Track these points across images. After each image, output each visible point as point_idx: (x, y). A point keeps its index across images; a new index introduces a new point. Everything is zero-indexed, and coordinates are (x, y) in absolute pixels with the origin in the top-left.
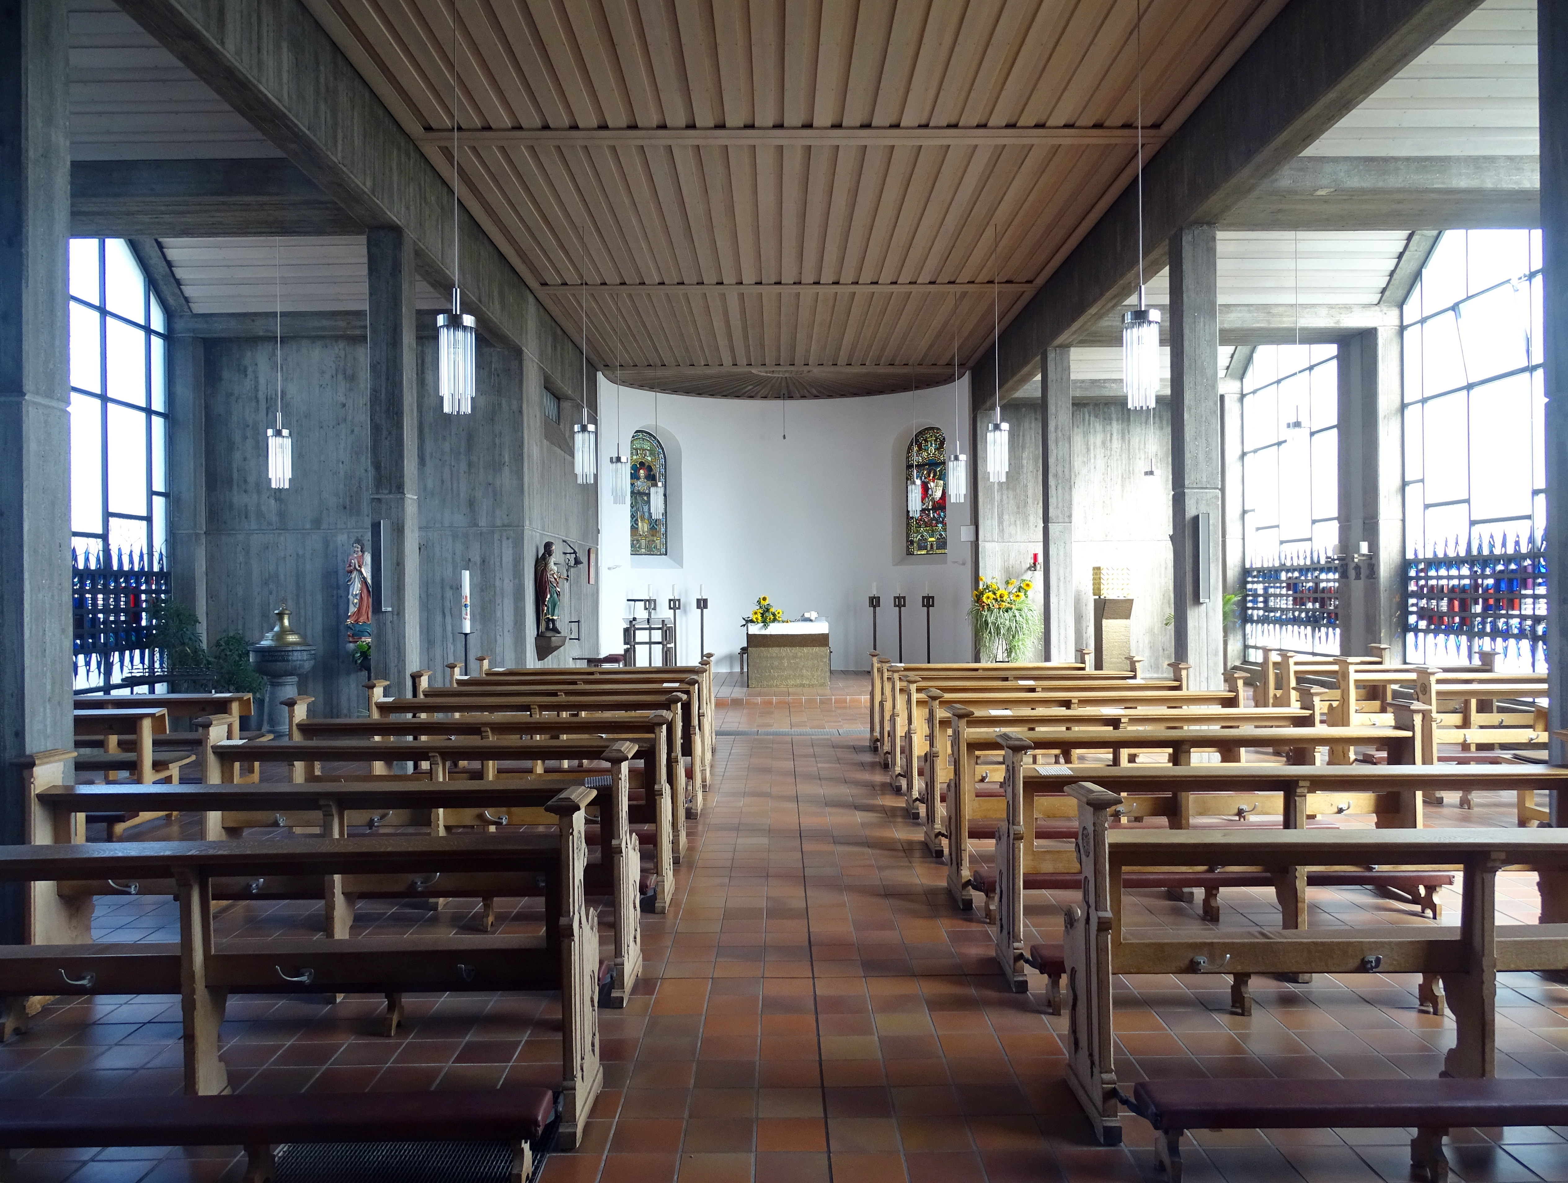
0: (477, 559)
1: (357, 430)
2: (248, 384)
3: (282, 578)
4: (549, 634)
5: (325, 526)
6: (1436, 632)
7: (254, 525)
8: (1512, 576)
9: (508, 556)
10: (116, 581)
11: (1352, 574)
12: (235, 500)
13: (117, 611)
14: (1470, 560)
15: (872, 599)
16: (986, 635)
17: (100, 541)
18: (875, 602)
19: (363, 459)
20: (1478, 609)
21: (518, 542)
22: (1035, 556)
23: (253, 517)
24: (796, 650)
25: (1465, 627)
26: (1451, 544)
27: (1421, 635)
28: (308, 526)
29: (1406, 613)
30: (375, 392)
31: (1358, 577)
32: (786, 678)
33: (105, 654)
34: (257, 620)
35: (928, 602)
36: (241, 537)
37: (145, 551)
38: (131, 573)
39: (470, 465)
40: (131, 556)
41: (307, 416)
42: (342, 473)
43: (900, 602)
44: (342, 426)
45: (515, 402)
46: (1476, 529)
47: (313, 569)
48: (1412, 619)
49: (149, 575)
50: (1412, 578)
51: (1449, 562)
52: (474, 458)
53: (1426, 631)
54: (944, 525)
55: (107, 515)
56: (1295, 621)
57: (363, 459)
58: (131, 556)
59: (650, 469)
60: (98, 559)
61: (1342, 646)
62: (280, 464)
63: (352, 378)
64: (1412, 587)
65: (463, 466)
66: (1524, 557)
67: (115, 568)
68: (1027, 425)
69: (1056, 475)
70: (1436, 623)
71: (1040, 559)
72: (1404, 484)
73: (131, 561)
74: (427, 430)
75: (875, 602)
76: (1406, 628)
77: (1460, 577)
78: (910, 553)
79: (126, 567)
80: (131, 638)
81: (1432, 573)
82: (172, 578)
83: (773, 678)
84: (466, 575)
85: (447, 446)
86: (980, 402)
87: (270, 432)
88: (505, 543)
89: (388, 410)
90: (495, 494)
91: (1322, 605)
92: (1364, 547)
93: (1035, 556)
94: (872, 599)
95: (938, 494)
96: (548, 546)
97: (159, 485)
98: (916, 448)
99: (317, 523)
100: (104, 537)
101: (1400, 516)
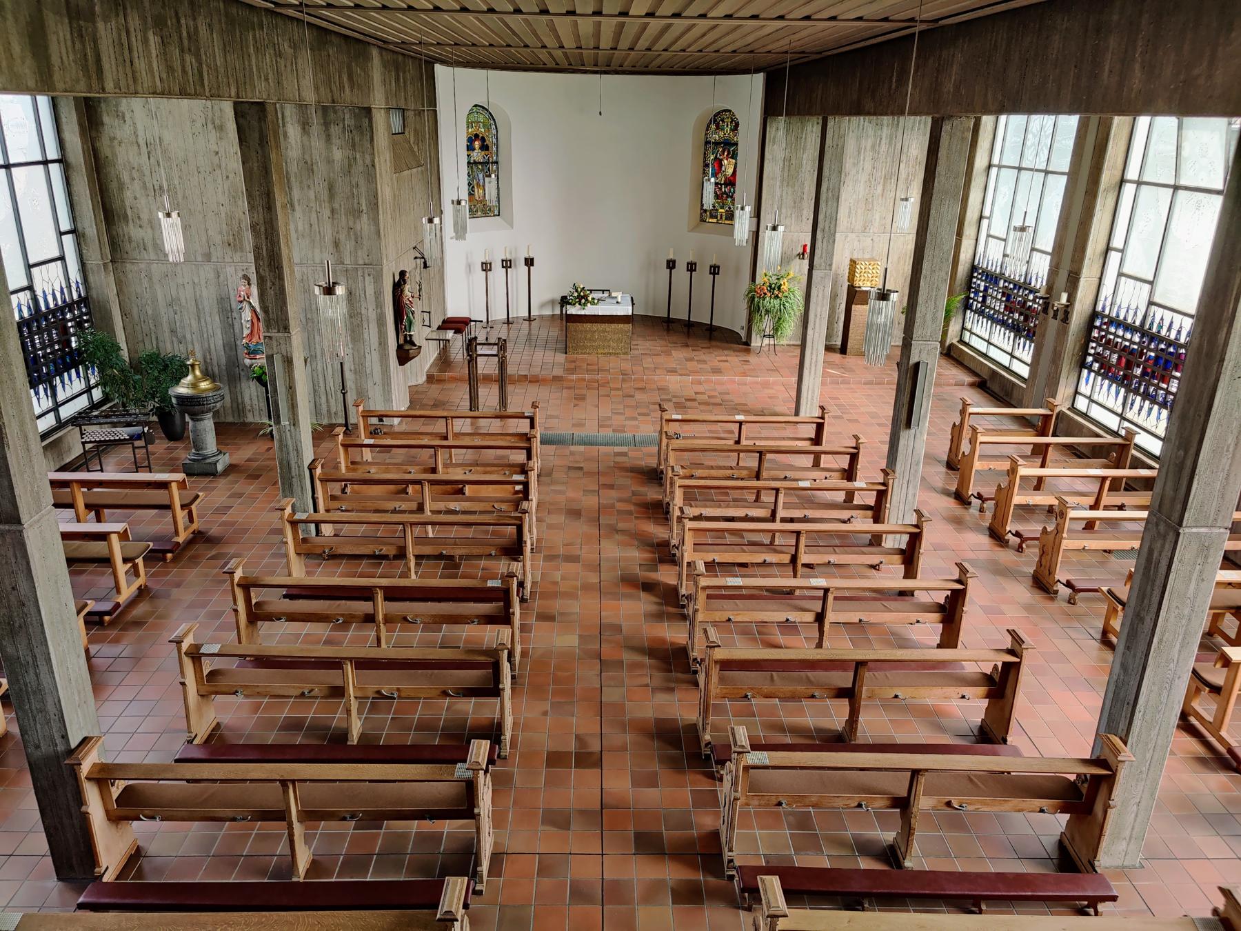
3: (183, 301)
4: (407, 347)
5: (214, 259)
6: (1105, 377)
7: (153, 256)
8: (1169, 357)
9: (370, 290)
10: (46, 319)
11: (1051, 313)
12: (133, 234)
14: (1142, 330)
15: (668, 262)
16: (757, 316)
17: (28, 292)
18: (671, 264)
19: (240, 203)
20: (1138, 371)
21: (378, 279)
22: (805, 246)
23: (150, 249)
24: (604, 326)
25: (1124, 381)
26: (1131, 313)
27: (1093, 374)
28: (200, 259)
29: (1086, 354)
30: (257, 249)
31: (1055, 317)
34: (167, 334)
35: (715, 270)
36: (143, 266)
39: (333, 211)
40: (54, 294)
41: (186, 161)
42: (223, 215)
43: (691, 267)
44: (218, 172)
45: (367, 157)
46: (1154, 308)
47: (209, 296)
48: (1090, 359)
49: (70, 306)
51: (1128, 327)
52: (336, 206)
53: (1098, 373)
54: (733, 200)
55: (29, 267)
56: (1003, 323)
57: (240, 203)
58: (54, 294)
59: (483, 139)
60: (29, 308)
61: (1033, 357)
62: (172, 236)
63: (221, 128)
64: (1095, 334)
65: (328, 212)
66: (1181, 346)
67: (43, 309)
68: (809, 128)
69: (823, 230)
70: (1106, 371)
71: (808, 250)
73: (55, 298)
76: (1082, 365)
77: (1130, 341)
78: (703, 220)
79: (52, 306)
80: (68, 361)
81: (1112, 330)
83: (586, 347)
87: (161, 215)
88: (367, 278)
89: (270, 265)
91: (1026, 319)
93: (805, 246)
94: (668, 262)
95: (730, 171)
96: (403, 273)
97: (65, 225)
98: (714, 127)
99: (208, 257)
100: (30, 288)
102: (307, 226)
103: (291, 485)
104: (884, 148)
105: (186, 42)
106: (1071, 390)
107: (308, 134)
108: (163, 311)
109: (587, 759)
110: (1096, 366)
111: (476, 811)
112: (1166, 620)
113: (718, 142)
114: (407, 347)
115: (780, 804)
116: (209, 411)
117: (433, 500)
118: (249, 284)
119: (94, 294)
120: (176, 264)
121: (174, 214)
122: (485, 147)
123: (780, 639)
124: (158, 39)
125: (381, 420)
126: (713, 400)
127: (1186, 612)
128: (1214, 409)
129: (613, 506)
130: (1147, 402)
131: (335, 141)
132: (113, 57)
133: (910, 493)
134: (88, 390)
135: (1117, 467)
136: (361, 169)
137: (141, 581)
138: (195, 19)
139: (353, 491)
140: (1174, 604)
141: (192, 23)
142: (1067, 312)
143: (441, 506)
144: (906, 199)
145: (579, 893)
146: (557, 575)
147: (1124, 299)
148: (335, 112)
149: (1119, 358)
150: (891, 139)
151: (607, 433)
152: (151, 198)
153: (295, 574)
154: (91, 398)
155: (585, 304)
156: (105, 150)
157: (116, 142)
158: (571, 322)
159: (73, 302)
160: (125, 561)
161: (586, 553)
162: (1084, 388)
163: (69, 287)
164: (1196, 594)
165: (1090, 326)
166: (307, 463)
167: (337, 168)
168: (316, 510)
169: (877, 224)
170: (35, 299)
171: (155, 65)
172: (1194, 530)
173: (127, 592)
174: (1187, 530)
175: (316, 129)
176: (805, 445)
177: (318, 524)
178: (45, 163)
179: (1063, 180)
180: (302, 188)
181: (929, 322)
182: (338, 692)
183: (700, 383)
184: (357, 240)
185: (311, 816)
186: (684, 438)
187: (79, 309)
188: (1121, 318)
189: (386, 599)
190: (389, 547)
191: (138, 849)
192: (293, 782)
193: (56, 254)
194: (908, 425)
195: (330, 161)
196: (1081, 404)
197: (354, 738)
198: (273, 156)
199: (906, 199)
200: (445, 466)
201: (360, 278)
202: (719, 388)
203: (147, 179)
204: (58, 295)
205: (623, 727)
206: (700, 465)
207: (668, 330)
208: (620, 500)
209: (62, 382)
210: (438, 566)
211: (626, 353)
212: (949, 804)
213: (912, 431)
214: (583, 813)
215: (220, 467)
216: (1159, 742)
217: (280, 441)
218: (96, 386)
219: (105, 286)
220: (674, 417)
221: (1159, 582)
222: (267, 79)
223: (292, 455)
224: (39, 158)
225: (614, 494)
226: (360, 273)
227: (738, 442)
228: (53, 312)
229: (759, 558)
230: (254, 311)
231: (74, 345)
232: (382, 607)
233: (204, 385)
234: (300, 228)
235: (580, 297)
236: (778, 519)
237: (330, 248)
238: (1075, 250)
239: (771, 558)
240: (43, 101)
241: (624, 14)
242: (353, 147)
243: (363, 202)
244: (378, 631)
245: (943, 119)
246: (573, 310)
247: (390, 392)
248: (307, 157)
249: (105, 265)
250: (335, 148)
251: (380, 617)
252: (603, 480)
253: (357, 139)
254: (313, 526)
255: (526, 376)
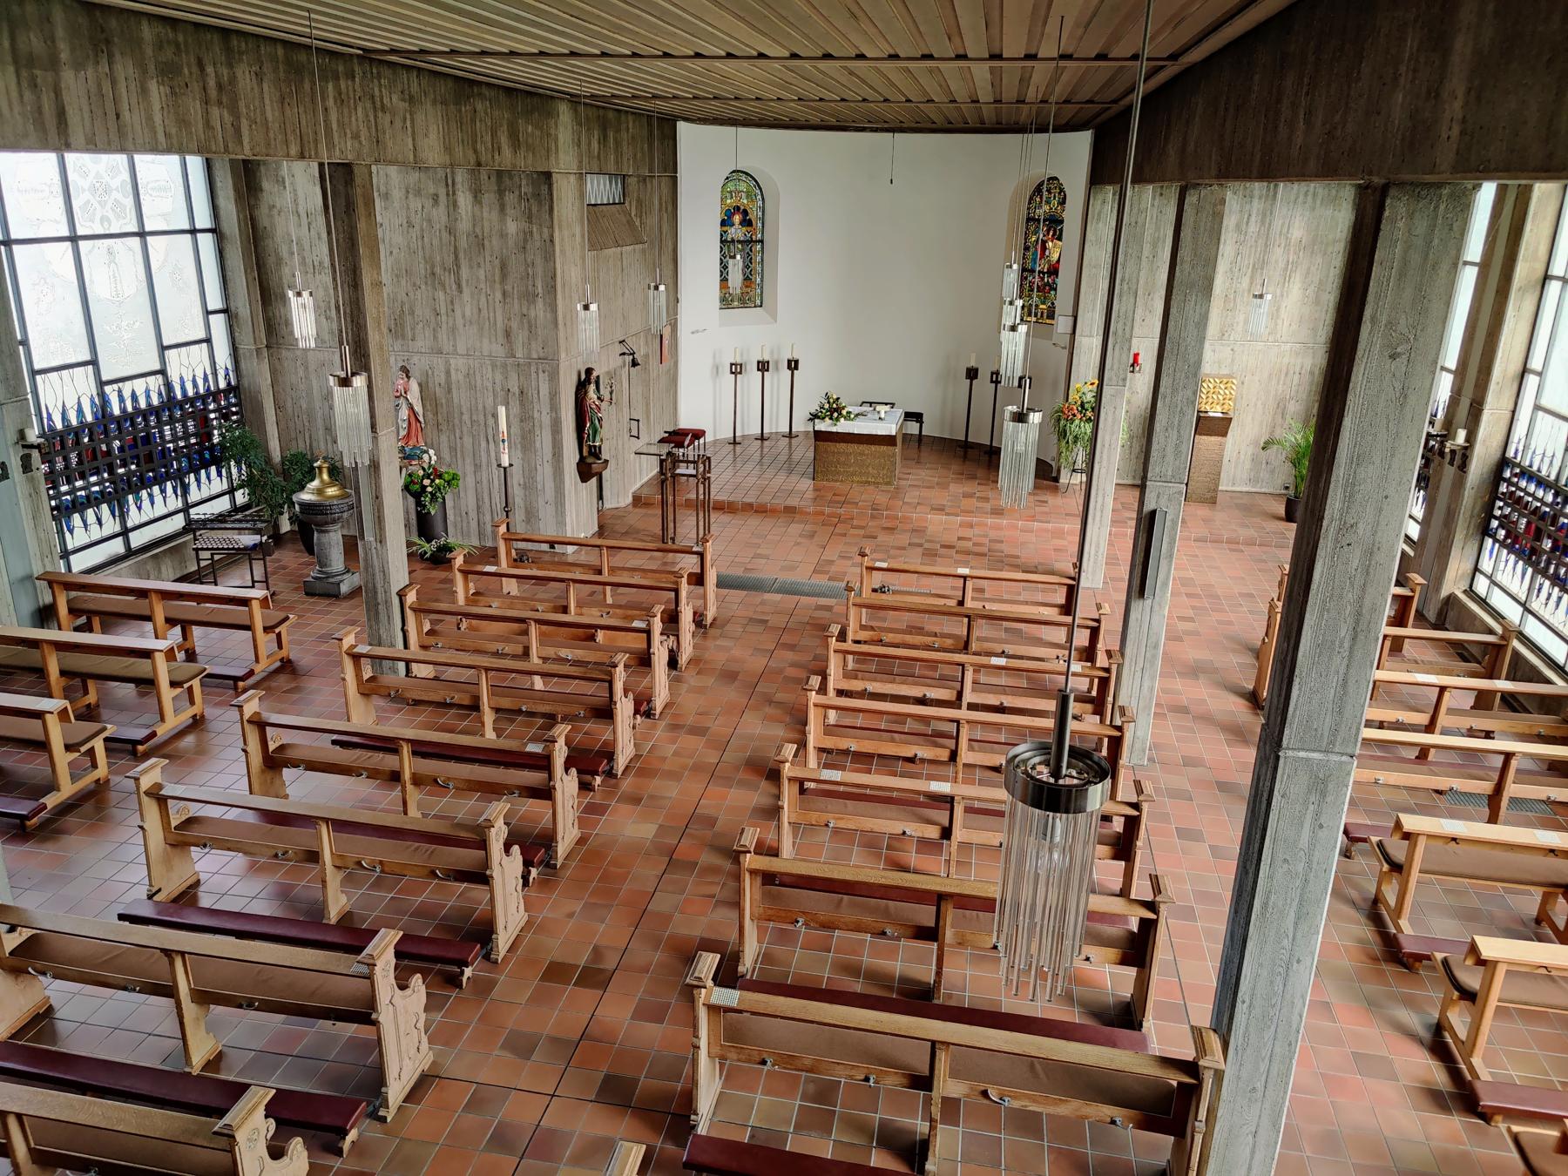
0: (516, 390)
1: (395, 251)
2: (288, 195)
4: (590, 460)
6: (1511, 549)
10: (182, 409)
13: (186, 436)
17: (160, 377)
18: (972, 374)
20: (1547, 544)
21: (554, 376)
24: (862, 447)
25: (1529, 556)
29: (1491, 516)
32: (853, 474)
33: (179, 477)
34: (321, 432)
37: (209, 372)
38: (198, 396)
39: (504, 294)
48: (1495, 523)
49: (215, 395)
50: (1505, 480)
51: (1542, 482)
52: (508, 288)
53: (1503, 544)
55: (163, 349)
59: (745, 213)
60: (160, 394)
64: (1503, 488)
65: (499, 295)
67: (179, 396)
70: (1513, 543)
72: (1525, 371)
74: (461, 255)
75: (972, 374)
76: (1485, 531)
79: (191, 393)
80: (206, 457)
81: (1523, 484)
82: (236, 396)
83: (838, 473)
84: (502, 411)
85: (481, 273)
86: (1103, 171)
87: (290, 294)
90: (530, 327)
92: (1461, 437)
95: (1055, 257)
97: (215, 302)
100: (162, 372)
101: (1511, 407)
102: (475, 311)
103: (377, 613)
104: (1253, 228)
105: (213, 93)
106: (1469, 566)
107: (480, 203)
108: (318, 404)
109: (594, 977)
110: (1502, 533)
111: (374, 1016)
112: (1271, 877)
113: (1042, 217)
114: (590, 460)
115: (764, 1062)
116: (334, 522)
117: (542, 643)
118: (408, 377)
119: (245, 382)
120: (306, 350)
121: (305, 294)
122: (747, 222)
123: (913, 858)
124: (165, 90)
125: (552, 547)
126: (977, 549)
127: (1300, 867)
128: (1314, 586)
129: (781, 671)
130: (1556, 589)
131: (510, 211)
132: (86, 108)
133: (1146, 684)
134: (231, 491)
135: (1491, 677)
136: (538, 244)
137: (196, 710)
138: (230, 66)
139: (470, 628)
140: (1280, 856)
141: (225, 72)
142: (1465, 455)
143: (550, 652)
144: (1261, 296)
145: (501, 1140)
146: (670, 750)
147: (1538, 443)
148: (511, 178)
149: (1529, 523)
150: (1264, 215)
151: (821, 581)
152: (310, 276)
153: (354, 719)
154: (233, 500)
155: (837, 419)
156: (264, 221)
157: (275, 212)
158: (829, 446)
159: (219, 391)
160: (173, 684)
161: (718, 726)
162: (1486, 564)
163: (215, 373)
164: (1312, 845)
165: (1497, 475)
166: (395, 589)
167: (511, 243)
168: (406, 646)
169: (1239, 328)
170: (168, 385)
171: (158, 118)
172: (1302, 754)
173: (174, 720)
174: (1290, 753)
175: (489, 198)
176: (1051, 613)
177: (408, 662)
178: (193, 232)
179: (1475, 270)
180: (471, 267)
181: (1170, 457)
182: (313, 857)
183: (971, 526)
184: (531, 328)
185: (204, 998)
186: (895, 592)
187: (227, 398)
188: (1535, 468)
189: (415, 753)
190: (462, 695)
191: (50, 1009)
192: (183, 954)
193: (202, 335)
194: (1141, 593)
195: (503, 235)
196: (1481, 585)
197: (333, 915)
198: (362, 226)
199: (1261, 296)
200: (579, 605)
201: (534, 375)
202: (993, 534)
203: (307, 254)
204: (200, 382)
205: (656, 943)
206: (920, 631)
207: (965, 458)
208: (792, 665)
209: (198, 481)
210: (530, 725)
211: (888, 483)
212: (985, 1094)
213: (1148, 602)
214: (554, 1041)
215: (344, 588)
216: (1278, 1050)
217: (366, 560)
218: (241, 487)
219: (259, 375)
220: (878, 564)
221: (1260, 824)
222: (356, 136)
223: (379, 577)
224: (187, 227)
225: (790, 656)
226: (533, 369)
227: (961, 603)
228: (192, 401)
229: (908, 751)
230: (411, 408)
231: (216, 440)
232: (408, 764)
233: (332, 491)
234: (468, 313)
235: (832, 411)
236: (964, 705)
237: (501, 339)
238: (1479, 371)
239: (924, 752)
240: (195, 163)
241: (1031, 57)
242: (530, 219)
243: (539, 284)
244: (404, 791)
245: (1384, 191)
246: (824, 426)
247: (563, 514)
248: (478, 230)
249: (258, 350)
250: (509, 220)
251: (407, 775)
252: (786, 639)
253: (534, 209)
254: (401, 666)
255: (751, 505)
